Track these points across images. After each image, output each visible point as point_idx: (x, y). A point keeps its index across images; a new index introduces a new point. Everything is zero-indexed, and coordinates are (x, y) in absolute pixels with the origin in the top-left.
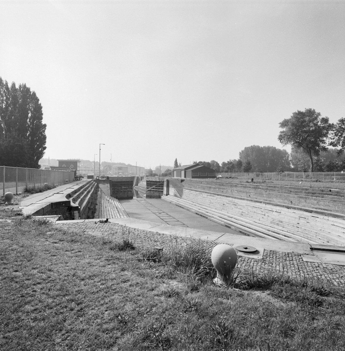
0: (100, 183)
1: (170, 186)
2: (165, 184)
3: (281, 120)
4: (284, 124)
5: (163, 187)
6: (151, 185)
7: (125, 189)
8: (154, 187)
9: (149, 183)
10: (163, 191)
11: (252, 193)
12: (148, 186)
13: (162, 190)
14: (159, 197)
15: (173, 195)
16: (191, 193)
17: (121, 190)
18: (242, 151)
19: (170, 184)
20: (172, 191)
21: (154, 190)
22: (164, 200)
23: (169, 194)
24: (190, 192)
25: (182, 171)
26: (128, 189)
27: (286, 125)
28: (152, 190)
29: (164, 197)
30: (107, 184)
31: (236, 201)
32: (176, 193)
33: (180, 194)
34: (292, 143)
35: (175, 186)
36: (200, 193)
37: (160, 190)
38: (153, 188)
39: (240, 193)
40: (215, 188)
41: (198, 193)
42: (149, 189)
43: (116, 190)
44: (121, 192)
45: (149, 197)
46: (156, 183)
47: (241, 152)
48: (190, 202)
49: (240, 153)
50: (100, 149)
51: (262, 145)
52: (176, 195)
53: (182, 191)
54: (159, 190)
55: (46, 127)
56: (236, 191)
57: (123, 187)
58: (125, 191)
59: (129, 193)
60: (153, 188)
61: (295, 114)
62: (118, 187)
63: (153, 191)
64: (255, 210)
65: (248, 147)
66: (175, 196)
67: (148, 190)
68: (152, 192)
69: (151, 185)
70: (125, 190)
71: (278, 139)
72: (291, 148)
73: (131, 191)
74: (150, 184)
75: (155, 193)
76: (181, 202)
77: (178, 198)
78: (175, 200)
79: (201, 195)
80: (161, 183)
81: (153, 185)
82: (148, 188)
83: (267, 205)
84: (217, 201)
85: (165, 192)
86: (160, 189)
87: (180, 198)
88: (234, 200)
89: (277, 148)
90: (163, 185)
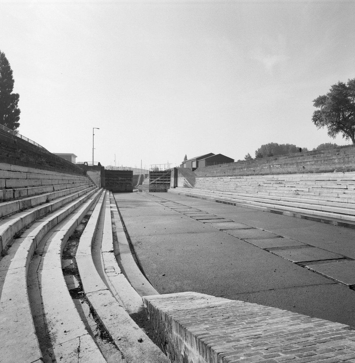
1: (178, 175)
2: (173, 173)
3: (316, 97)
4: (320, 101)
5: (170, 178)
6: (155, 177)
8: (159, 179)
9: (153, 174)
10: (170, 183)
11: (309, 162)
13: (169, 182)
14: (165, 191)
15: (183, 186)
16: (207, 180)
18: (258, 150)
19: (178, 173)
20: (181, 181)
21: (159, 182)
22: (170, 193)
23: (177, 187)
24: (205, 180)
25: (193, 162)
27: (322, 103)
28: (157, 182)
29: (170, 190)
30: (98, 171)
31: (281, 177)
32: (186, 183)
33: (192, 183)
34: (330, 125)
35: (185, 175)
36: (219, 178)
37: (166, 182)
38: (158, 181)
39: (285, 166)
40: (241, 168)
41: (217, 178)
43: (110, 181)
44: (118, 184)
45: (151, 191)
46: (161, 174)
47: (257, 151)
48: (206, 190)
49: (256, 152)
50: (94, 135)
51: (280, 143)
52: (186, 185)
53: (194, 180)
55: (19, 98)
56: (278, 165)
57: (120, 178)
58: (122, 183)
59: (128, 185)
60: (158, 181)
61: (335, 87)
63: (158, 184)
64: (319, 184)
65: (265, 144)
66: (186, 186)
67: (152, 184)
68: (156, 185)
69: (155, 177)
71: (312, 121)
72: (328, 131)
73: (130, 184)
75: (160, 186)
76: (194, 191)
77: (189, 189)
78: (186, 191)
79: (222, 180)
82: (151, 181)
83: (345, 173)
84: (247, 183)
85: (172, 184)
86: (166, 181)
87: (192, 188)
88: (275, 177)
89: (297, 146)
90: (170, 175)
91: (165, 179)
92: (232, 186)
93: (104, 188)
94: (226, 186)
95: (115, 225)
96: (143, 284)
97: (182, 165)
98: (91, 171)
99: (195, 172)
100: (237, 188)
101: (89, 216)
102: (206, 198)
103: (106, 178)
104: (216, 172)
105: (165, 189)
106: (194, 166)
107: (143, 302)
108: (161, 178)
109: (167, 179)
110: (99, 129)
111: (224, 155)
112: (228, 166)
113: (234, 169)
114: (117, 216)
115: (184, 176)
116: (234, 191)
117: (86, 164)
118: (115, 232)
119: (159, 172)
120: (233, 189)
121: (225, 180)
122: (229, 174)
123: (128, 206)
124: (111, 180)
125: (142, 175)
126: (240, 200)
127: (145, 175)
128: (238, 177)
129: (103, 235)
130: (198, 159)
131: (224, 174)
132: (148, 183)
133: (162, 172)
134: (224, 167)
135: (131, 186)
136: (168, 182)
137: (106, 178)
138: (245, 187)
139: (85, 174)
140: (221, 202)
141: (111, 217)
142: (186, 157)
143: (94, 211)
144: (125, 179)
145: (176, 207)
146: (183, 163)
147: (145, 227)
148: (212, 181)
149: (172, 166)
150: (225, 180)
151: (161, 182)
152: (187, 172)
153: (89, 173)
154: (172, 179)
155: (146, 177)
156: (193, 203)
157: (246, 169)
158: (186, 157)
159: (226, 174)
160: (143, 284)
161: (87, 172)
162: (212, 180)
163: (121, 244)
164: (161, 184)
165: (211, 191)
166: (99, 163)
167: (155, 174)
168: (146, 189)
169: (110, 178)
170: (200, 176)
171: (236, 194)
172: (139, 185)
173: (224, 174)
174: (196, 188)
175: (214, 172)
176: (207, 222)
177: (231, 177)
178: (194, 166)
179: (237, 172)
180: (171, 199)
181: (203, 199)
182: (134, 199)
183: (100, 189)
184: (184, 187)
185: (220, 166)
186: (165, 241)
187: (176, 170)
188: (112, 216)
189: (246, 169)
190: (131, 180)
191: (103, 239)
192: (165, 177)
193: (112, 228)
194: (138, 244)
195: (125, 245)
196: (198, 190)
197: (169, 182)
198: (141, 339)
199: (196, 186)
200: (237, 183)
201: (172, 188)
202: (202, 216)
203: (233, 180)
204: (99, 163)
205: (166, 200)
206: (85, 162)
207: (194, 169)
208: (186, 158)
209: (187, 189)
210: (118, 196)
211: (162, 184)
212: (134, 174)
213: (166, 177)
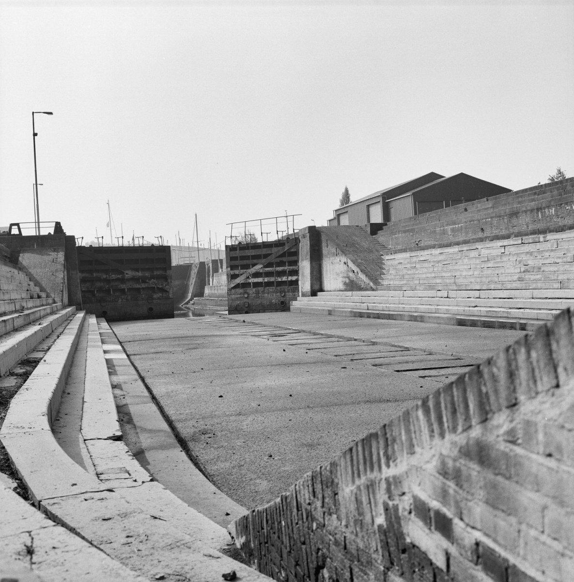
0: (24, 251)
1: (325, 251)
2: (305, 247)
5: (296, 263)
6: (245, 262)
7: (135, 279)
8: (258, 268)
9: (238, 253)
10: (297, 281)
12: (232, 268)
13: (294, 278)
14: (284, 307)
15: (342, 287)
16: (422, 259)
17: (123, 286)
19: (324, 244)
20: (336, 269)
21: (260, 280)
22: (300, 311)
23: (322, 290)
25: (372, 209)
26: (152, 283)
29: (300, 303)
30: (54, 251)
32: (351, 274)
33: (373, 272)
36: (465, 248)
37: (284, 279)
38: (256, 275)
40: (539, 209)
41: (455, 249)
42: (238, 281)
43: (98, 284)
44: (123, 291)
45: (234, 310)
46: (265, 251)
48: (420, 293)
50: (35, 135)
52: (352, 282)
54: (280, 280)
57: (129, 274)
58: (138, 290)
59: (155, 296)
60: (256, 275)
62: (106, 272)
63: (256, 285)
66: (352, 286)
67: (237, 286)
68: (252, 291)
69: (245, 262)
70: (138, 286)
73: (162, 290)
74: (243, 258)
75: (263, 292)
79: (473, 254)
80: (286, 248)
81: (255, 261)
84: (561, 254)
85: (305, 284)
86: (283, 273)
87: (373, 290)
90: (296, 254)
91: (280, 269)
92: (510, 270)
93: (79, 309)
94: (489, 272)
95: (122, 389)
96: (228, 514)
97: (336, 221)
98: (33, 251)
99: (381, 237)
100: (527, 276)
101: (35, 362)
102: (422, 317)
103: (84, 275)
104: (453, 230)
105: (282, 303)
106: (377, 216)
107: (233, 538)
108: (265, 267)
109: (287, 268)
110: (51, 113)
111: (472, 175)
112: (493, 207)
113: (515, 214)
114: (126, 375)
115: (344, 253)
116: (517, 285)
117: (15, 231)
118: (125, 405)
119: (256, 246)
120: (515, 278)
121: (485, 252)
122: (496, 232)
123: (159, 350)
124: (99, 280)
125: (202, 264)
126: (542, 311)
127: (211, 265)
128: (530, 239)
129: (84, 405)
130: (388, 197)
131: (480, 235)
132: (224, 290)
133: (266, 245)
134: (479, 211)
135: (168, 298)
136: (290, 278)
137: (84, 275)
138: (553, 268)
139: (13, 261)
140: (474, 324)
141: (109, 372)
142: (346, 196)
143: (49, 353)
144: (147, 274)
145: (322, 346)
146: (339, 214)
147: (221, 396)
148: (438, 262)
149: (301, 224)
150: (485, 252)
151: (266, 280)
152: (354, 238)
153: (26, 259)
154: (305, 266)
155: (216, 270)
156: (381, 332)
157: (553, 211)
158: (346, 196)
159: (487, 233)
160: (228, 514)
161: (21, 255)
162: (441, 258)
163: (144, 430)
164: (266, 286)
165: (439, 294)
166: (58, 226)
167: (242, 254)
168: (219, 308)
169: (95, 275)
170: (399, 247)
171: (528, 293)
172: (191, 299)
173: (480, 235)
174: (388, 288)
175: (444, 232)
176: (431, 374)
177: (505, 242)
178: (377, 216)
179: (524, 222)
180: (303, 328)
181: (414, 319)
182: (180, 333)
183: (64, 307)
184: (346, 290)
185: (466, 210)
186: (291, 423)
187: (314, 233)
188: (111, 370)
189: (553, 211)
190: (165, 278)
191: (84, 414)
192: (278, 260)
193: (115, 397)
194: (203, 437)
195: (159, 431)
196: (392, 293)
197: (294, 278)
198: (234, 573)
199: (385, 283)
200: (524, 257)
201: (304, 295)
202: (413, 362)
203: (513, 250)
204: (58, 226)
205: (290, 329)
206: (12, 225)
207: (376, 229)
208: (348, 197)
209: (357, 295)
210: (124, 330)
211: (269, 284)
212: (175, 262)
213: (284, 259)
